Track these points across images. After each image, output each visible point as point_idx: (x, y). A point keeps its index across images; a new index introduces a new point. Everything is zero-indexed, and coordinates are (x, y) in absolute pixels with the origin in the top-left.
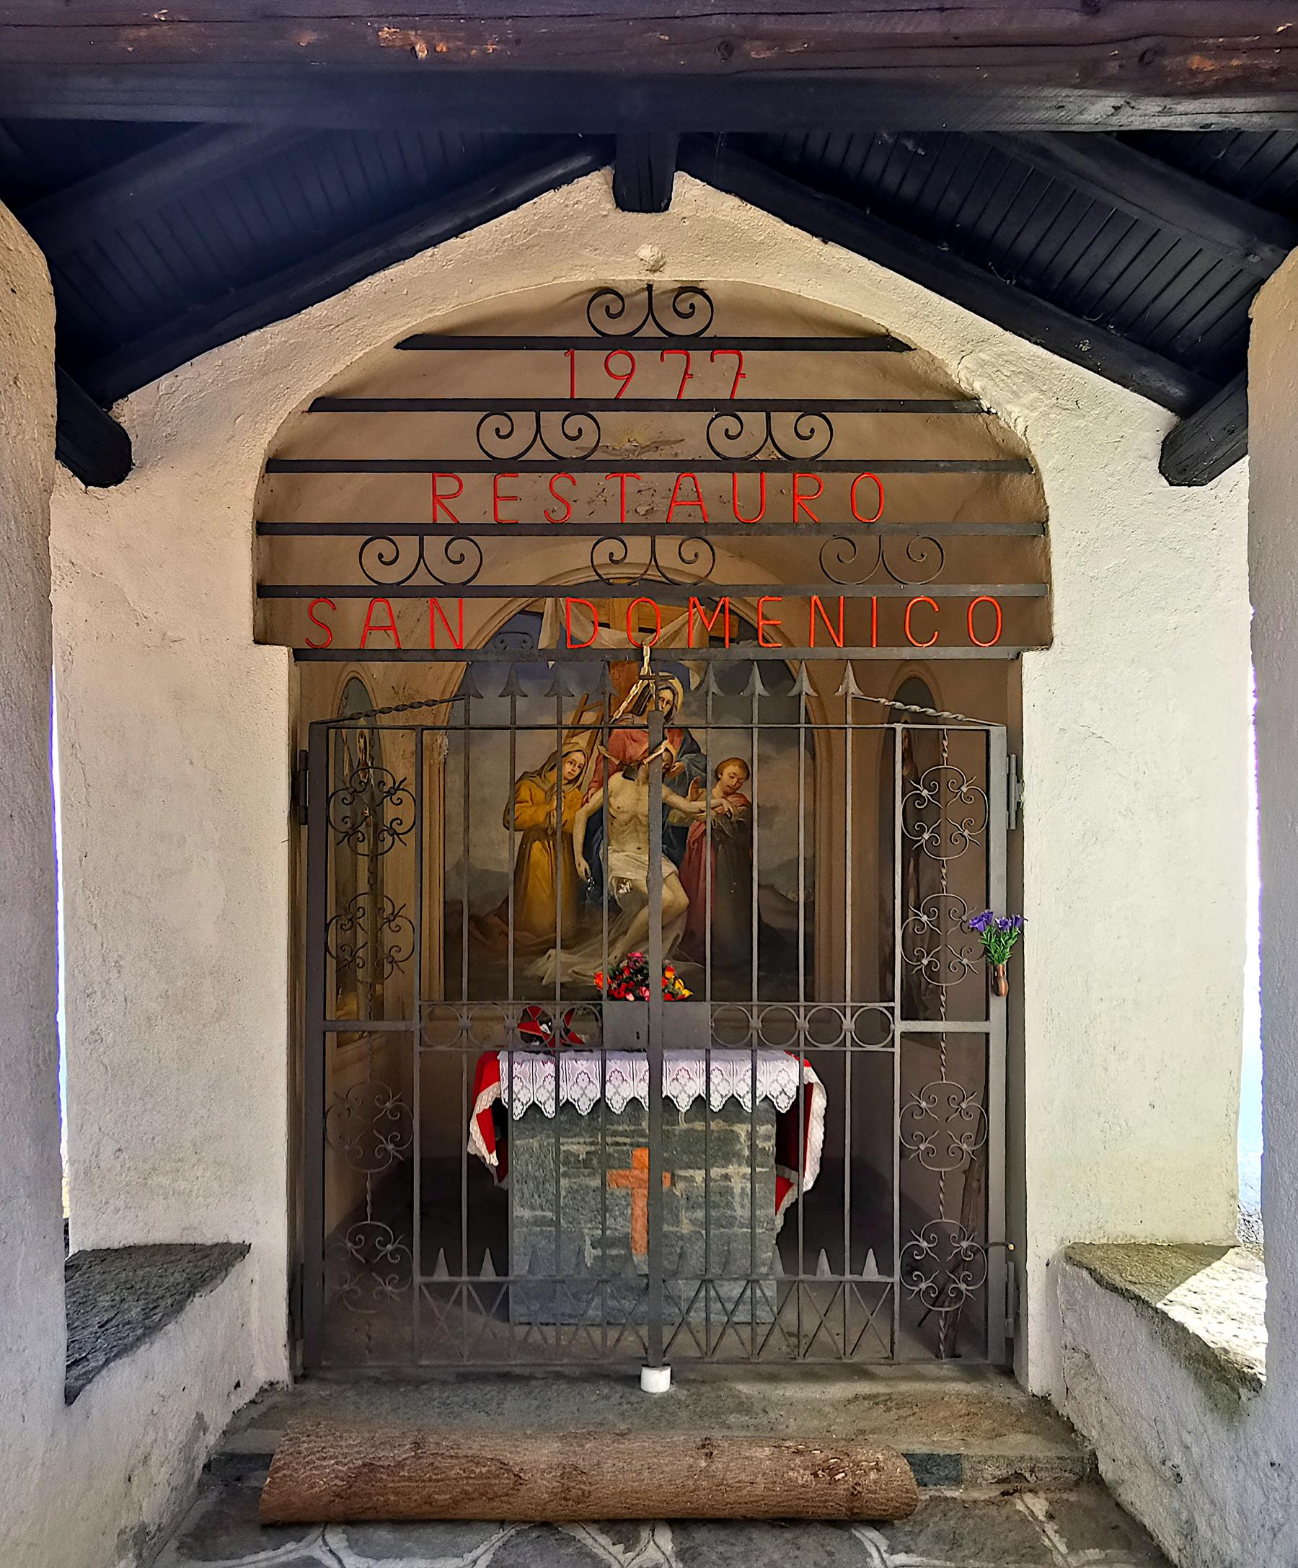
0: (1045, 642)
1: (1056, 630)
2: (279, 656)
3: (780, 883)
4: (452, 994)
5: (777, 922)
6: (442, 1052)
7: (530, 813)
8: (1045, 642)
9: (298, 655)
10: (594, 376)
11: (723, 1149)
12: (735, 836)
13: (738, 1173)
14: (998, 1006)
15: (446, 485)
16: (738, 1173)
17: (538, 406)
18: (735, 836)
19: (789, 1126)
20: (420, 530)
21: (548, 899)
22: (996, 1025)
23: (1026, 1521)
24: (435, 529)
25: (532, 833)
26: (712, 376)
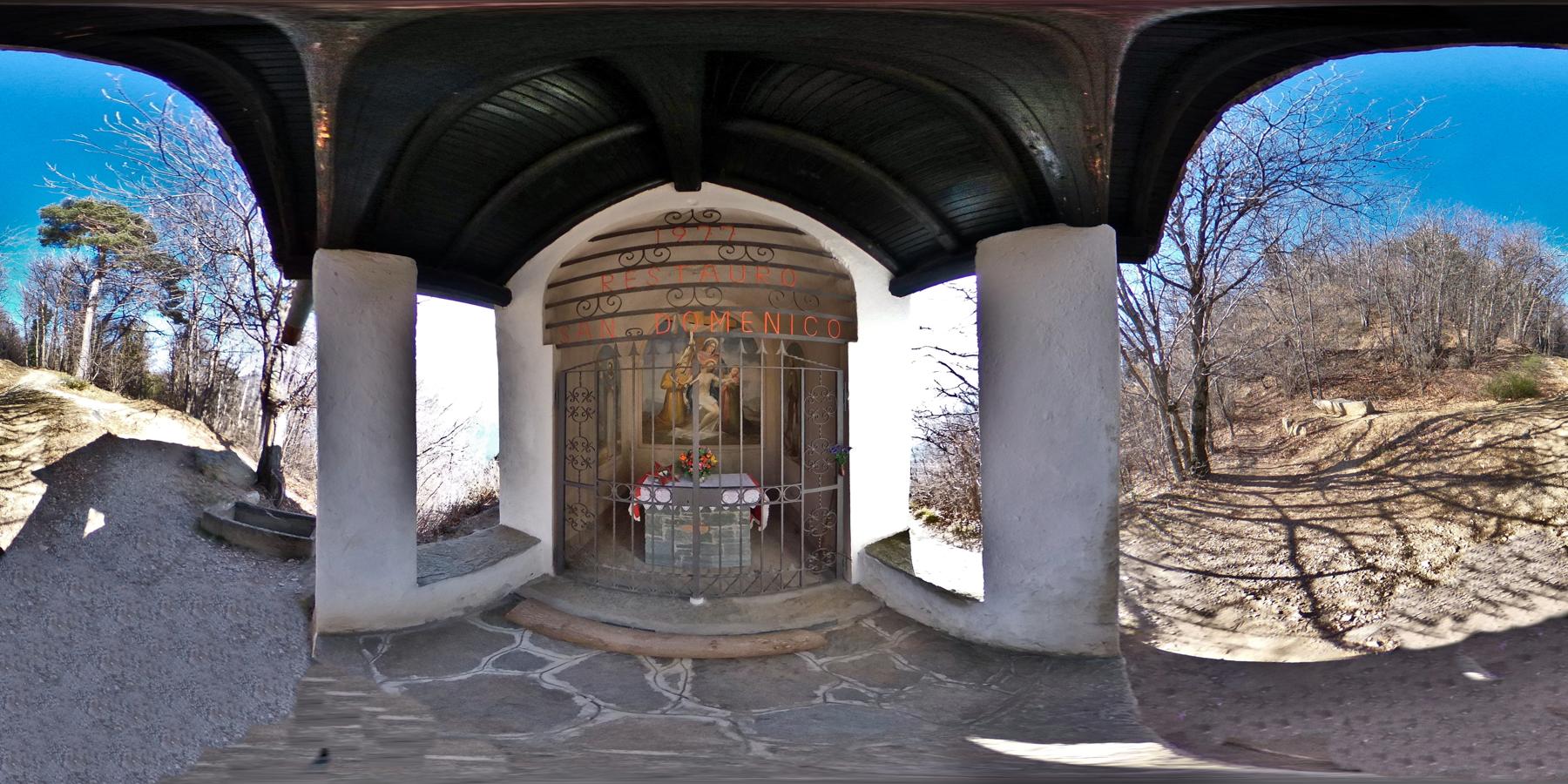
0: (855, 339)
1: (916, 297)
2: (550, 347)
3: (751, 406)
4: (647, 440)
5: (750, 419)
6: (1052, 147)
7: (668, 383)
8: (855, 339)
9: (558, 347)
10: (666, 236)
11: (730, 519)
12: (734, 391)
13: (735, 528)
14: (840, 479)
15: (607, 278)
16: (735, 528)
17: (643, 248)
18: (734, 391)
19: (756, 512)
20: (598, 296)
21: (674, 414)
22: (839, 486)
23: (868, 630)
24: (604, 294)
25: (669, 390)
26: (717, 234)
